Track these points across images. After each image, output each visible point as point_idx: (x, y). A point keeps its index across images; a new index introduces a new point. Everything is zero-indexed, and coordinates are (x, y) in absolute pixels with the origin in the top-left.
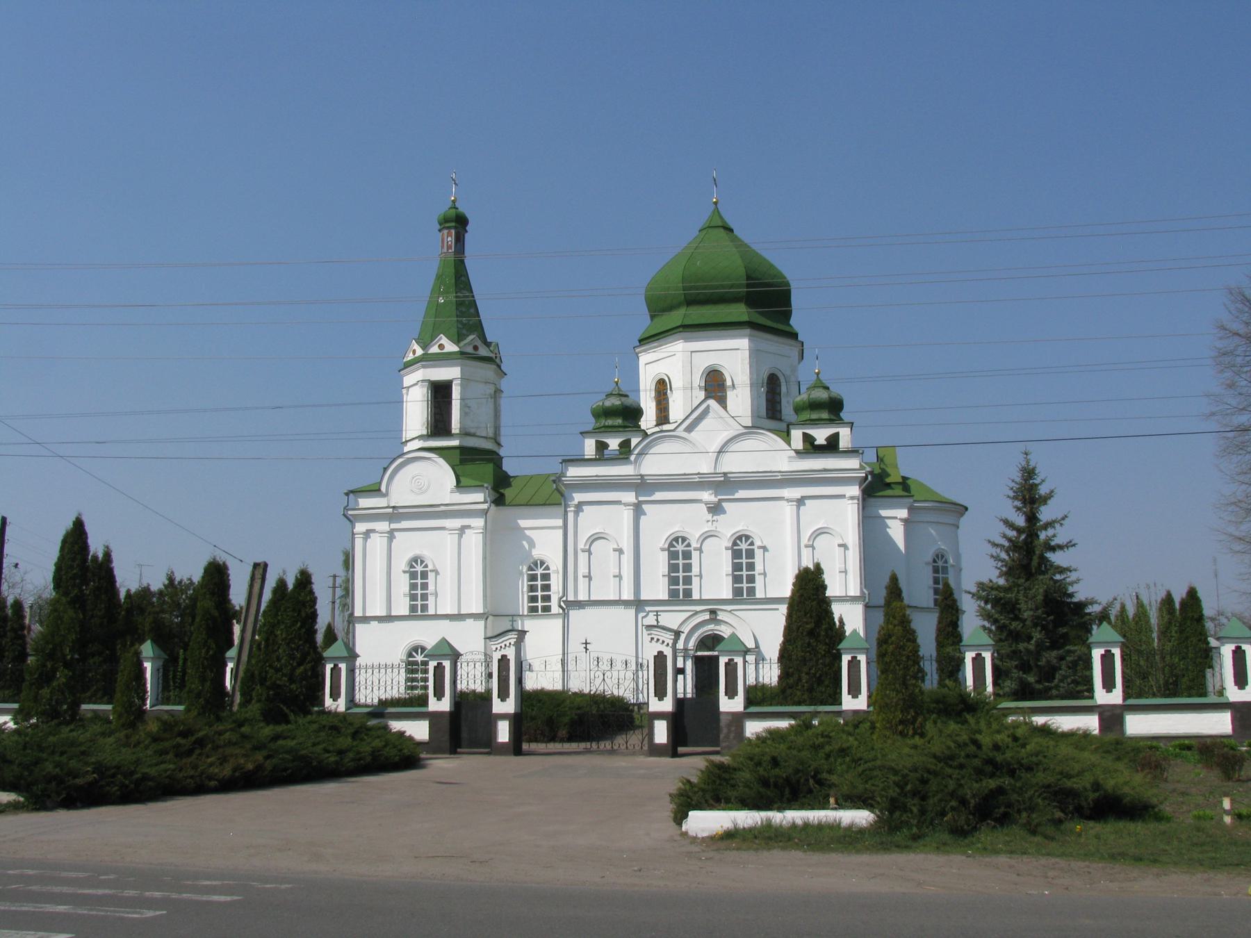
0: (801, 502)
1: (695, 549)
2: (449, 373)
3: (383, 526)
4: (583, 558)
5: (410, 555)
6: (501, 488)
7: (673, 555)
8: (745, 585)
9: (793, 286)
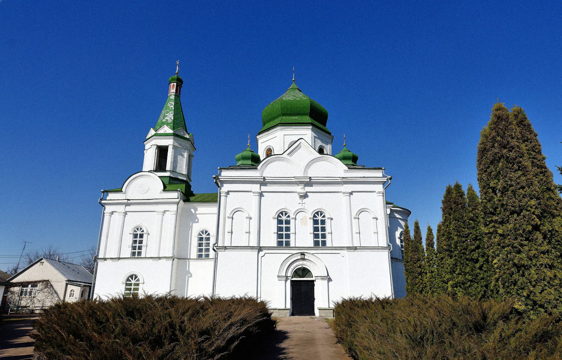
2: (168, 142)
3: (121, 209)
4: (229, 221)
6: (188, 196)
7: (280, 222)
8: (320, 240)
9: (329, 115)
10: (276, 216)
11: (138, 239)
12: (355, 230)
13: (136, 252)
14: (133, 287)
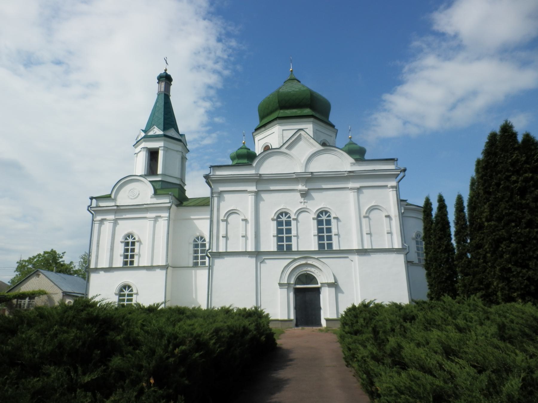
0: (359, 190)
1: (294, 219)
3: (112, 217)
4: (223, 225)
5: (126, 232)
7: (280, 224)
8: (326, 242)
10: (275, 218)
11: (130, 247)
12: (365, 230)
13: (129, 263)
14: (126, 298)
